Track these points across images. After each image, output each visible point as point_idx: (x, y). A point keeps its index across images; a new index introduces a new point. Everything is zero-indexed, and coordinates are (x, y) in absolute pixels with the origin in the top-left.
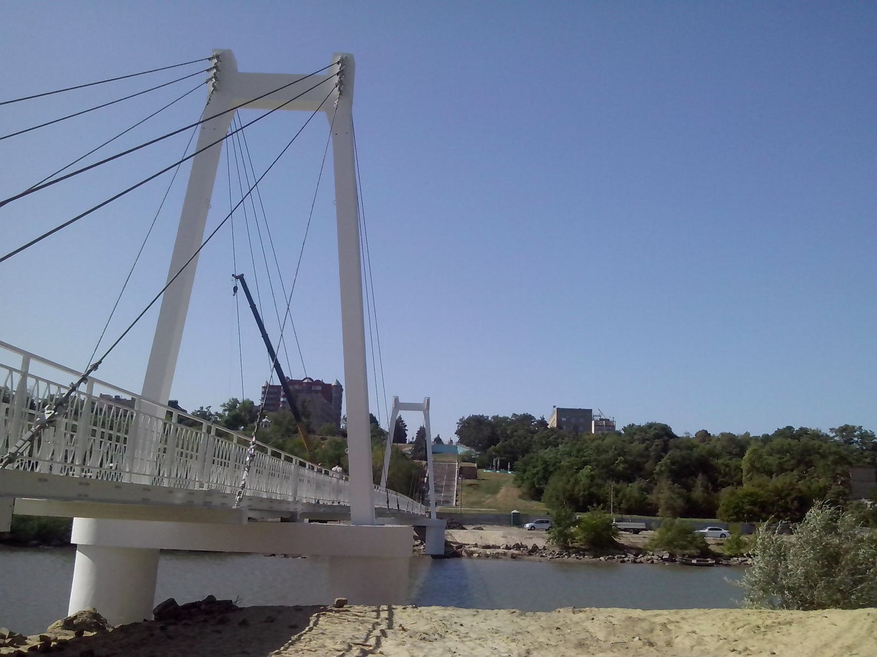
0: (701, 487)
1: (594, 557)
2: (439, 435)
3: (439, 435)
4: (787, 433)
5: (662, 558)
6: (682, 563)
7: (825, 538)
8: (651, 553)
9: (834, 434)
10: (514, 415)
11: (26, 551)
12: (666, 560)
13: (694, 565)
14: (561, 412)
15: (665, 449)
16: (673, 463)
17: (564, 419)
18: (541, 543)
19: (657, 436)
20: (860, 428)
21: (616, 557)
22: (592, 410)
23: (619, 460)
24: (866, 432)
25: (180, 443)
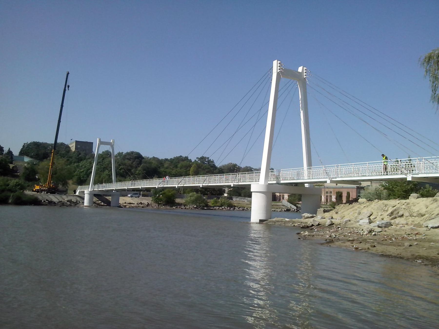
0: (234, 185)
1: (171, 207)
2: (9, 148)
3: (9, 148)
4: (138, 152)
5: (194, 207)
6: (201, 209)
7: (224, 200)
8: (189, 205)
9: (198, 160)
10: (176, 156)
11: (265, 206)
12: (195, 208)
13: (206, 209)
14: (77, 142)
15: (140, 163)
16: (144, 170)
17: (79, 146)
18: (150, 202)
19: (136, 158)
20: (208, 158)
21: (178, 207)
22: (93, 143)
23: (120, 168)
24: (210, 160)
25: (224, 177)
